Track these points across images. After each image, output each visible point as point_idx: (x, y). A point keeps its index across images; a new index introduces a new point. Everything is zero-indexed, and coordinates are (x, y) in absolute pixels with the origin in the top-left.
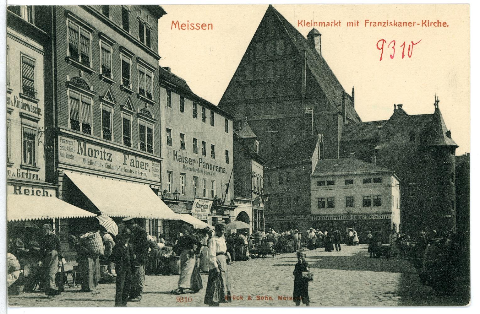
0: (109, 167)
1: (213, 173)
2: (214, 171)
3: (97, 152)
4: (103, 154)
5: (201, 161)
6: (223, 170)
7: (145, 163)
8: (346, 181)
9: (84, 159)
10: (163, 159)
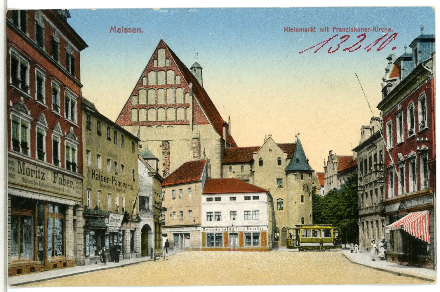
0: (43, 185)
1: (123, 190)
2: (124, 188)
3: (33, 172)
4: (38, 173)
5: (113, 180)
6: (131, 187)
7: (71, 181)
8: (231, 198)
9: (23, 178)
10: (84, 177)
